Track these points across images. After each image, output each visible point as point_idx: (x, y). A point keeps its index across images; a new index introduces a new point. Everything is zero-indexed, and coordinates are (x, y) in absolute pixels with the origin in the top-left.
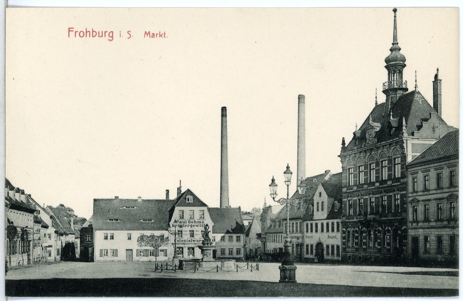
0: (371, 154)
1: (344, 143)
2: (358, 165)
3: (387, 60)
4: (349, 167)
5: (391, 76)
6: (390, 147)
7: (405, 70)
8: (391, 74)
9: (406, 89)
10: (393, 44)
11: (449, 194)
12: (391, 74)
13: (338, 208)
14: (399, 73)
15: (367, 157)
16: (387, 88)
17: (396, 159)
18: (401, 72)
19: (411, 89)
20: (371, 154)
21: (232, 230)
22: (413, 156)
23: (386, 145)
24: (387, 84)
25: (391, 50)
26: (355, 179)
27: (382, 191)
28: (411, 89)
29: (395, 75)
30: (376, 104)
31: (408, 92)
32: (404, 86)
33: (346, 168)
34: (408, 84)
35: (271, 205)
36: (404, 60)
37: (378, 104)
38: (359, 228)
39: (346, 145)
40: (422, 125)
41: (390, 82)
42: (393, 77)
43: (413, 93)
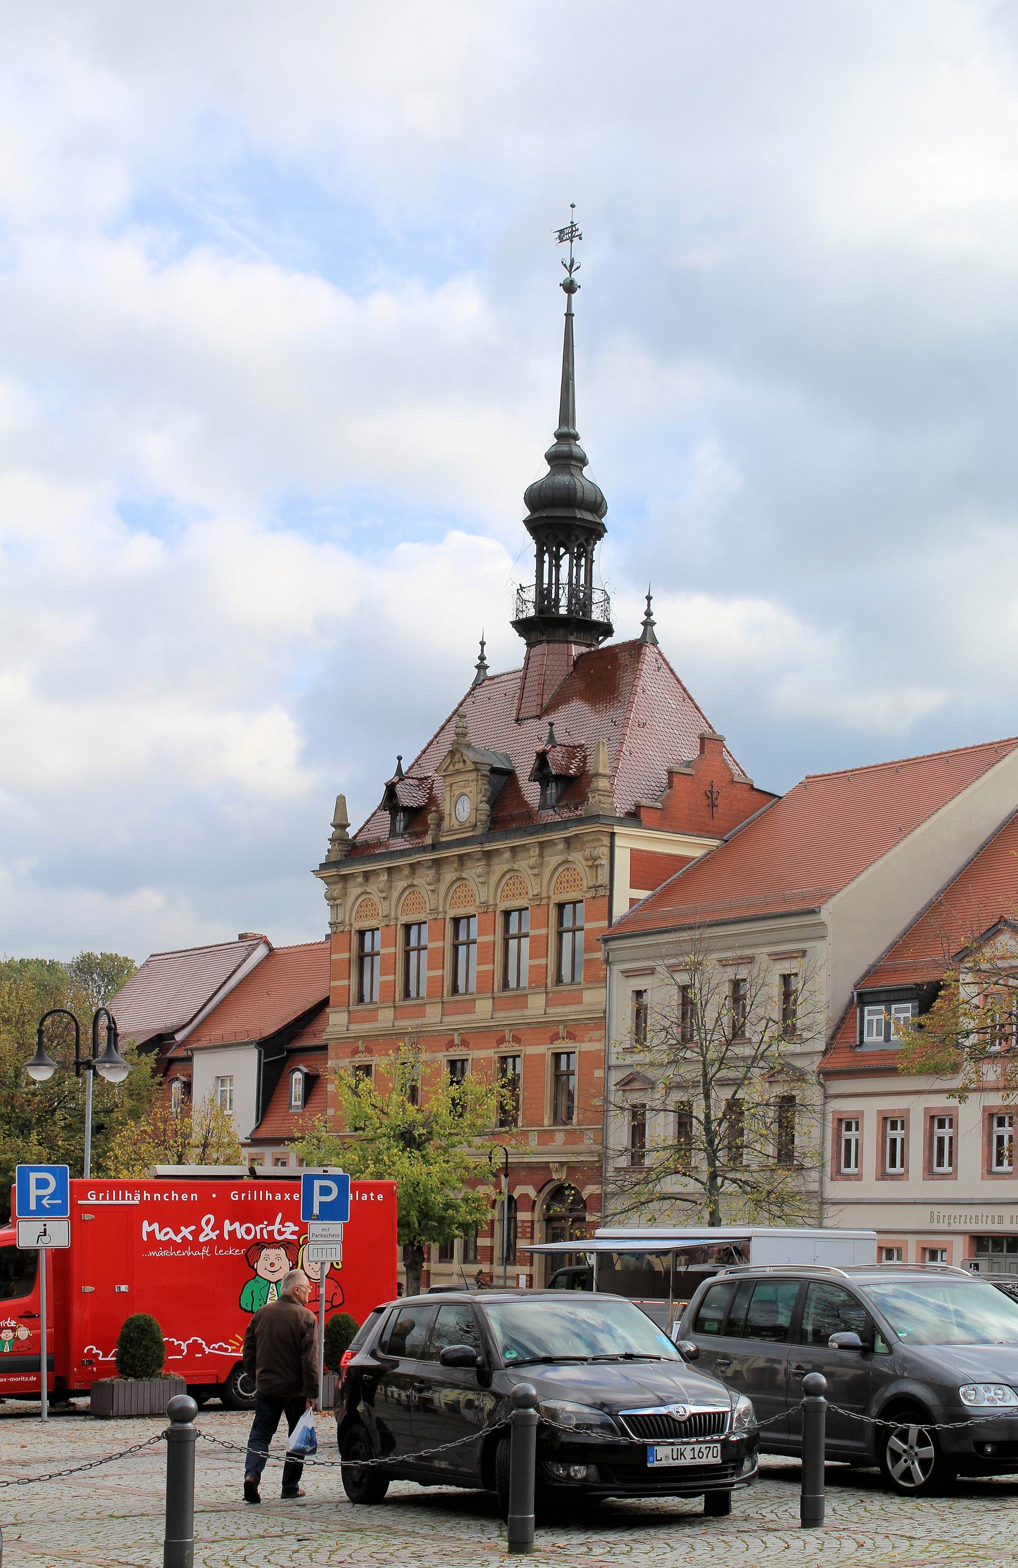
1: (341, 825)
2: (449, 911)
4: (366, 924)
6: (541, 855)
7: (603, 551)
9: (607, 630)
10: (559, 436)
11: (627, 1072)
15: (395, 894)
16: (531, 612)
17: (462, 921)
20: (566, 862)
21: (496, 1189)
22: (633, 902)
23: (524, 845)
24: (531, 595)
25: (552, 458)
26: (432, 973)
27: (504, 1037)
30: (481, 667)
31: (609, 642)
32: (596, 615)
33: (347, 928)
36: (598, 506)
37: (489, 673)
38: (497, 1185)
39: (351, 832)
43: (635, 648)
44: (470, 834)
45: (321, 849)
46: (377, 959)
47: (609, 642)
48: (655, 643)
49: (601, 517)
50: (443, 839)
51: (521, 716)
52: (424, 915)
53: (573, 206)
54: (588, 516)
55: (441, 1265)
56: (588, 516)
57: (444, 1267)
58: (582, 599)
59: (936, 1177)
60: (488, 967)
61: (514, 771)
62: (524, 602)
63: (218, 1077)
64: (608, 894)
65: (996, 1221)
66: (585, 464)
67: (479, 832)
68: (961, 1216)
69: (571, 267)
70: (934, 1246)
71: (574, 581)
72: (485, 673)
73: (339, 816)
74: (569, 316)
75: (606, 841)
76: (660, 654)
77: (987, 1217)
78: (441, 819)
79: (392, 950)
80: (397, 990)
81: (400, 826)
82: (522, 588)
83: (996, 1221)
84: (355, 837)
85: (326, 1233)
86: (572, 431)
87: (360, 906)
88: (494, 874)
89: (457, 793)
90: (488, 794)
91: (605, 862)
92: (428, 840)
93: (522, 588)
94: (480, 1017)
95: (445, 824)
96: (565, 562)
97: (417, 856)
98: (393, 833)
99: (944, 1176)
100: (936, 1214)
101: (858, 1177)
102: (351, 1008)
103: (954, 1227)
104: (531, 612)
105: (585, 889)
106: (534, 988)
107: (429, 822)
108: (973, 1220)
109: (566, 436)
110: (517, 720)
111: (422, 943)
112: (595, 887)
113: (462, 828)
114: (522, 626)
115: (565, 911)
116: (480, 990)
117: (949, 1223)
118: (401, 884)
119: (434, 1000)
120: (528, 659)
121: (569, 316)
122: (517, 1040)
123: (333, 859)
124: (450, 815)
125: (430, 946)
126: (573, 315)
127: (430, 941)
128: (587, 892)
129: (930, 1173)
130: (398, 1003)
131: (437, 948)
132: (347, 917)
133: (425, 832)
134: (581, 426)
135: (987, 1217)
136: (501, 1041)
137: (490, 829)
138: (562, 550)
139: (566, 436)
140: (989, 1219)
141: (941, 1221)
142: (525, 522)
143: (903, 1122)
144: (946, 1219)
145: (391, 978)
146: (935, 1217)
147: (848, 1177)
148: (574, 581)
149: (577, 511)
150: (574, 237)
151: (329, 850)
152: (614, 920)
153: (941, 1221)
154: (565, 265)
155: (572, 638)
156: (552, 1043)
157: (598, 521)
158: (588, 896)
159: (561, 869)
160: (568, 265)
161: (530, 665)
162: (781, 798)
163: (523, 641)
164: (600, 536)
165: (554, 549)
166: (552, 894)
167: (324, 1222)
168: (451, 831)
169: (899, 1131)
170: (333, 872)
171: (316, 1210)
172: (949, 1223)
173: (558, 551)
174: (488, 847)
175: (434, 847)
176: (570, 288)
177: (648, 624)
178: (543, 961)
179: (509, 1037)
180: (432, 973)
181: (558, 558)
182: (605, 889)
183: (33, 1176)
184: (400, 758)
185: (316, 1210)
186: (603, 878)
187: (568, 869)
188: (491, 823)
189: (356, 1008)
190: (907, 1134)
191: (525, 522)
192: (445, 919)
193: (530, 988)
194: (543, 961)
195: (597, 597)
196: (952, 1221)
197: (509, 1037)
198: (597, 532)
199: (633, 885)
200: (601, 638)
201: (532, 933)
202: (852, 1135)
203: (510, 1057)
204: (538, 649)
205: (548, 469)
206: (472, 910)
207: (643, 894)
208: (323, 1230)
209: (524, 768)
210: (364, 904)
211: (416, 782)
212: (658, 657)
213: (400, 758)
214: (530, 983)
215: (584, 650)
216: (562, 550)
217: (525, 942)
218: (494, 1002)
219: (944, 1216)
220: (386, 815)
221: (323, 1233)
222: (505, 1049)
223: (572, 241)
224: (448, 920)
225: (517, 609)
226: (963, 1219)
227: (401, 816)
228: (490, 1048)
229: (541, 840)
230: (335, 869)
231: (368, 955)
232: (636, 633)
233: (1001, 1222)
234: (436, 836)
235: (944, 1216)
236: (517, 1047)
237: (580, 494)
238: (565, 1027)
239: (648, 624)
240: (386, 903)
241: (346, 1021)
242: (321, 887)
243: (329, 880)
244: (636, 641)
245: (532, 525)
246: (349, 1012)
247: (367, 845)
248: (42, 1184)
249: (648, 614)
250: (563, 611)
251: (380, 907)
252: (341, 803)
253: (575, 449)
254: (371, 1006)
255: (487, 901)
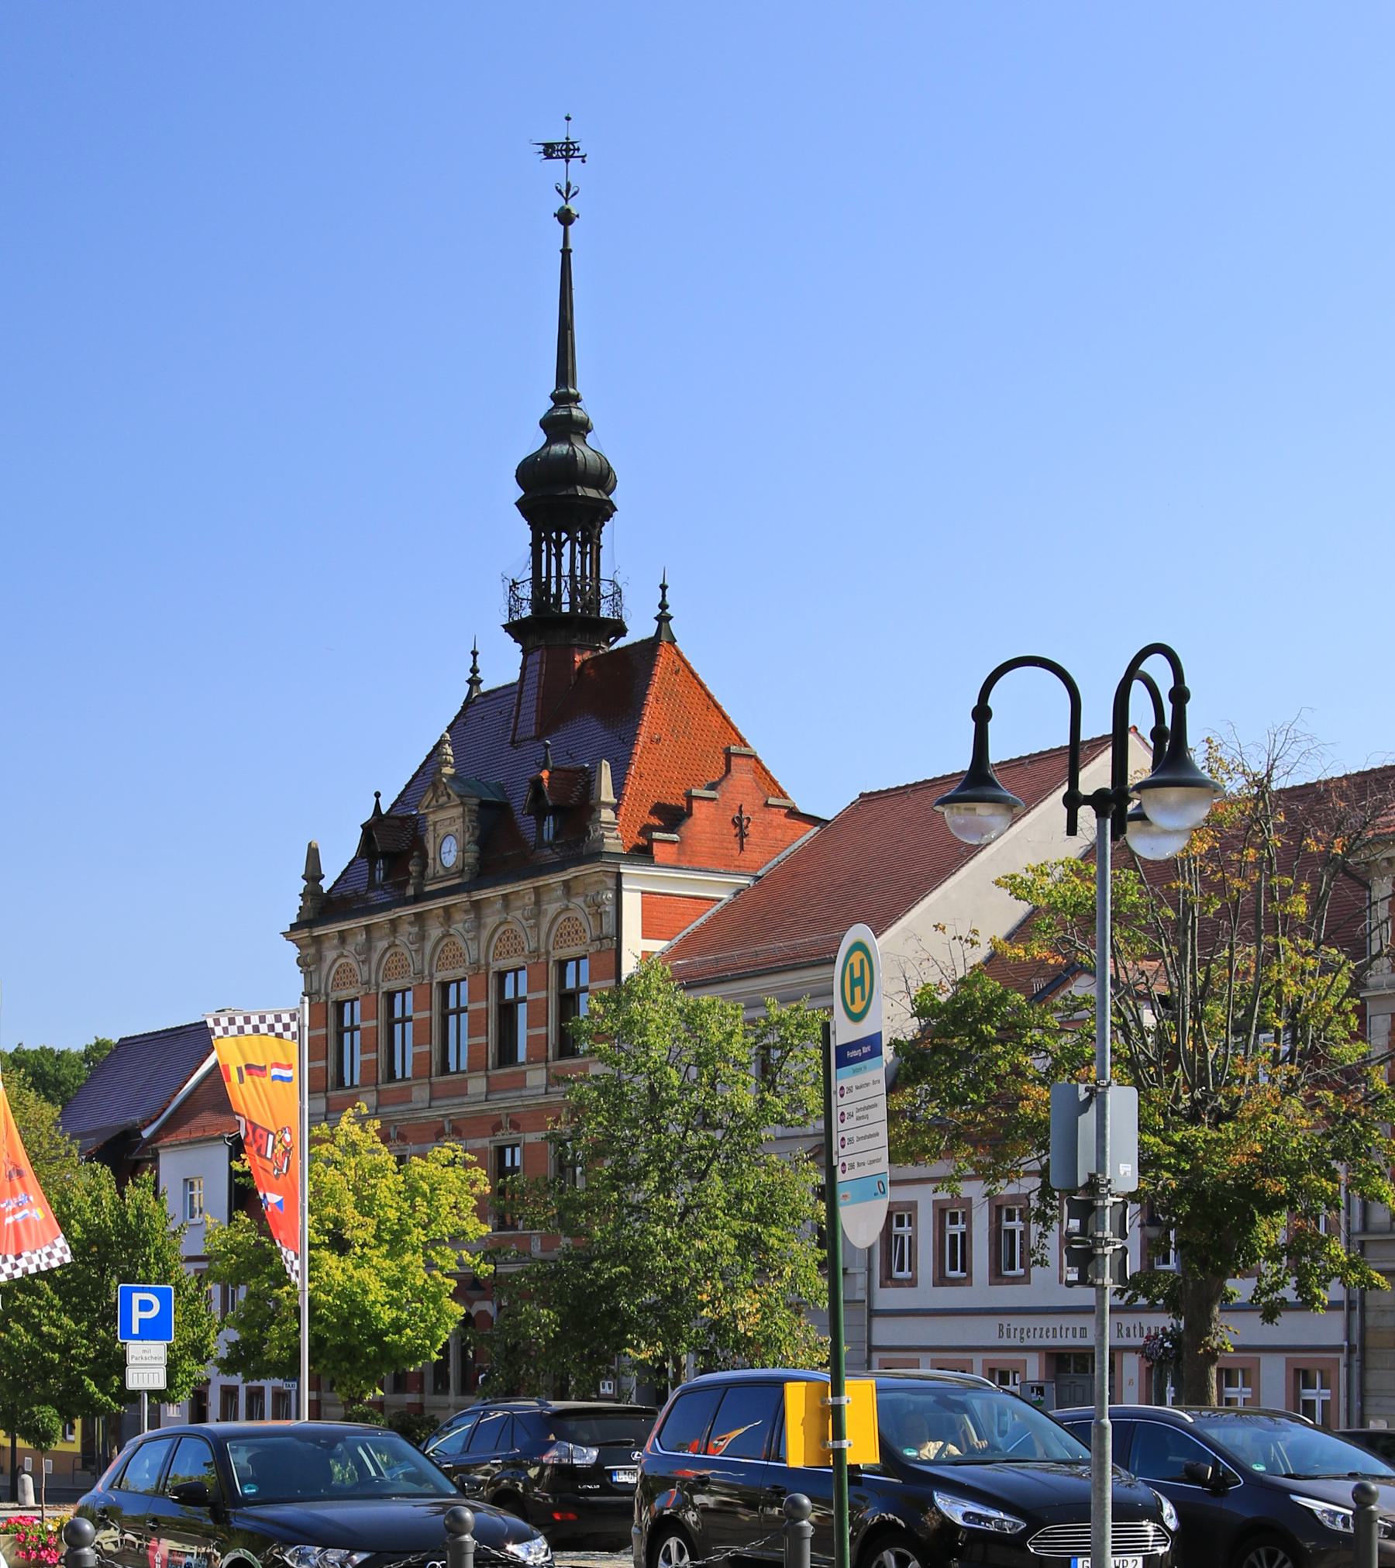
0: (392, 945)
1: (313, 874)
2: (382, 984)
3: (530, 473)
5: (544, 555)
7: (609, 533)
8: (544, 547)
12: (544, 547)
13: (773, 1242)
14: (583, 545)
16: (527, 612)
17: (570, 963)
18: (591, 542)
19: (639, 628)
20: (567, 909)
24: (526, 592)
25: (547, 424)
26: (418, 1049)
27: (444, 1128)
28: (639, 628)
29: (563, 551)
30: (474, 682)
31: (622, 643)
32: (605, 612)
34: (627, 601)
35: (868, 1245)
36: (603, 478)
37: (484, 688)
39: (326, 884)
40: (690, 807)
41: (539, 586)
42: (553, 559)
43: (649, 649)
44: (457, 881)
45: (291, 908)
46: (357, 1034)
47: (622, 643)
48: (672, 641)
49: (608, 494)
50: (428, 889)
51: (517, 738)
52: (522, 959)
53: (568, 119)
54: (592, 493)
55: (396, 1396)
56: (592, 493)
57: (438, 1399)
58: (588, 588)
59: (1005, 1281)
60: (482, 1040)
61: (508, 804)
62: (519, 600)
63: (186, 1180)
64: (614, 947)
65: (1078, 1335)
66: (589, 431)
67: (466, 879)
68: (1035, 1329)
69: (567, 192)
70: (1004, 1367)
71: (578, 572)
72: (478, 688)
73: (310, 868)
74: (566, 253)
75: (611, 883)
76: (679, 654)
77: (1067, 1329)
78: (425, 866)
79: (373, 1023)
80: (380, 1071)
81: (380, 875)
82: (515, 584)
83: (1078, 1335)
84: (330, 891)
85: (148, 1355)
86: (572, 390)
87: (337, 972)
88: (485, 926)
89: (442, 832)
90: (477, 833)
91: (610, 908)
92: (410, 891)
93: (515, 584)
94: (473, 1099)
95: (430, 871)
96: (566, 550)
97: (573, 869)
98: (372, 885)
99: (1015, 1280)
100: (1005, 1327)
101: (912, 1283)
102: (434, 1080)
103: (1027, 1342)
104: (527, 612)
105: (589, 941)
106: (533, 1063)
107: (411, 869)
108: (1051, 1334)
109: (564, 397)
110: (513, 742)
111: (407, 1014)
112: (600, 939)
113: (449, 873)
114: (515, 629)
115: (568, 969)
116: (472, 1069)
117: (1022, 1338)
118: (382, 945)
119: (420, 1081)
120: (523, 668)
121: (566, 253)
122: (515, 1126)
123: (305, 917)
124: (434, 859)
125: (593, 986)
126: (570, 251)
127: (592, 980)
128: (590, 945)
129: (997, 1276)
130: (382, 1087)
131: (423, 1019)
132: (323, 986)
133: (407, 882)
134: (583, 385)
135: (1067, 1329)
136: (497, 1127)
137: (479, 875)
138: (564, 536)
139: (564, 397)
140: (1070, 1332)
141: (1058, 1335)
142: (517, 504)
143: (910, 1217)
144: (1018, 1333)
145: (373, 1056)
146: (1005, 1331)
147: (900, 1283)
148: (578, 572)
149: (579, 488)
150: (572, 157)
151: (300, 908)
152: (624, 978)
153: (1058, 1335)
154: (560, 192)
155: (575, 641)
156: (494, 1135)
157: (605, 497)
158: (592, 950)
159: (388, 955)
160: (564, 190)
161: (527, 677)
162: (828, 822)
163: (519, 647)
164: (608, 517)
165: (554, 535)
166: (551, 949)
167: (145, 1342)
168: (436, 878)
169: (906, 1227)
170: (304, 933)
171: (135, 1330)
172: (1022, 1338)
173: (559, 536)
174: (477, 896)
175: (420, 897)
176: (565, 218)
177: (663, 619)
178: (543, 1031)
179: (506, 1123)
180: (418, 1049)
181: (560, 545)
182: (611, 939)
183: (137, 1297)
184: (377, 795)
185: (135, 1330)
186: (608, 928)
187: (569, 919)
188: (481, 867)
189: (385, 1087)
190: (969, 1227)
191: (517, 504)
192: (431, 984)
193: (529, 1063)
194: (543, 1031)
195: (606, 589)
196: (1025, 1335)
197: (506, 1123)
198: (604, 511)
199: (646, 935)
200: (611, 640)
201: (530, 997)
202: (905, 1230)
203: (508, 1146)
204: (536, 657)
205: (543, 438)
206: (460, 973)
207: (658, 946)
208: (144, 1351)
209: (520, 800)
210: (341, 970)
211: (398, 823)
212: (676, 657)
213: (377, 795)
214: (528, 1057)
215: (587, 655)
216: (564, 536)
217: (409, 1026)
218: (488, 1081)
219: (1015, 1329)
220: (364, 863)
221: (144, 1355)
222: (502, 1137)
223: (567, 161)
224: (434, 984)
225: (510, 610)
226: (1038, 1332)
227: (380, 864)
228: (484, 1137)
229: (537, 884)
230: (465, 895)
231: (398, 1021)
232: (649, 630)
233: (1084, 1336)
234: (419, 886)
235: (1015, 1329)
236: (516, 1135)
237: (581, 466)
238: (395, 1127)
239: (663, 619)
240: (365, 968)
241: (324, 1109)
242: (292, 951)
243: (304, 942)
244: (650, 639)
245: (524, 506)
246: (378, 1091)
247: (344, 900)
248: (145, 1306)
249: (663, 606)
250: (566, 609)
251: (358, 972)
252: (313, 855)
253: (575, 412)
254: (350, 1091)
255: (478, 960)
